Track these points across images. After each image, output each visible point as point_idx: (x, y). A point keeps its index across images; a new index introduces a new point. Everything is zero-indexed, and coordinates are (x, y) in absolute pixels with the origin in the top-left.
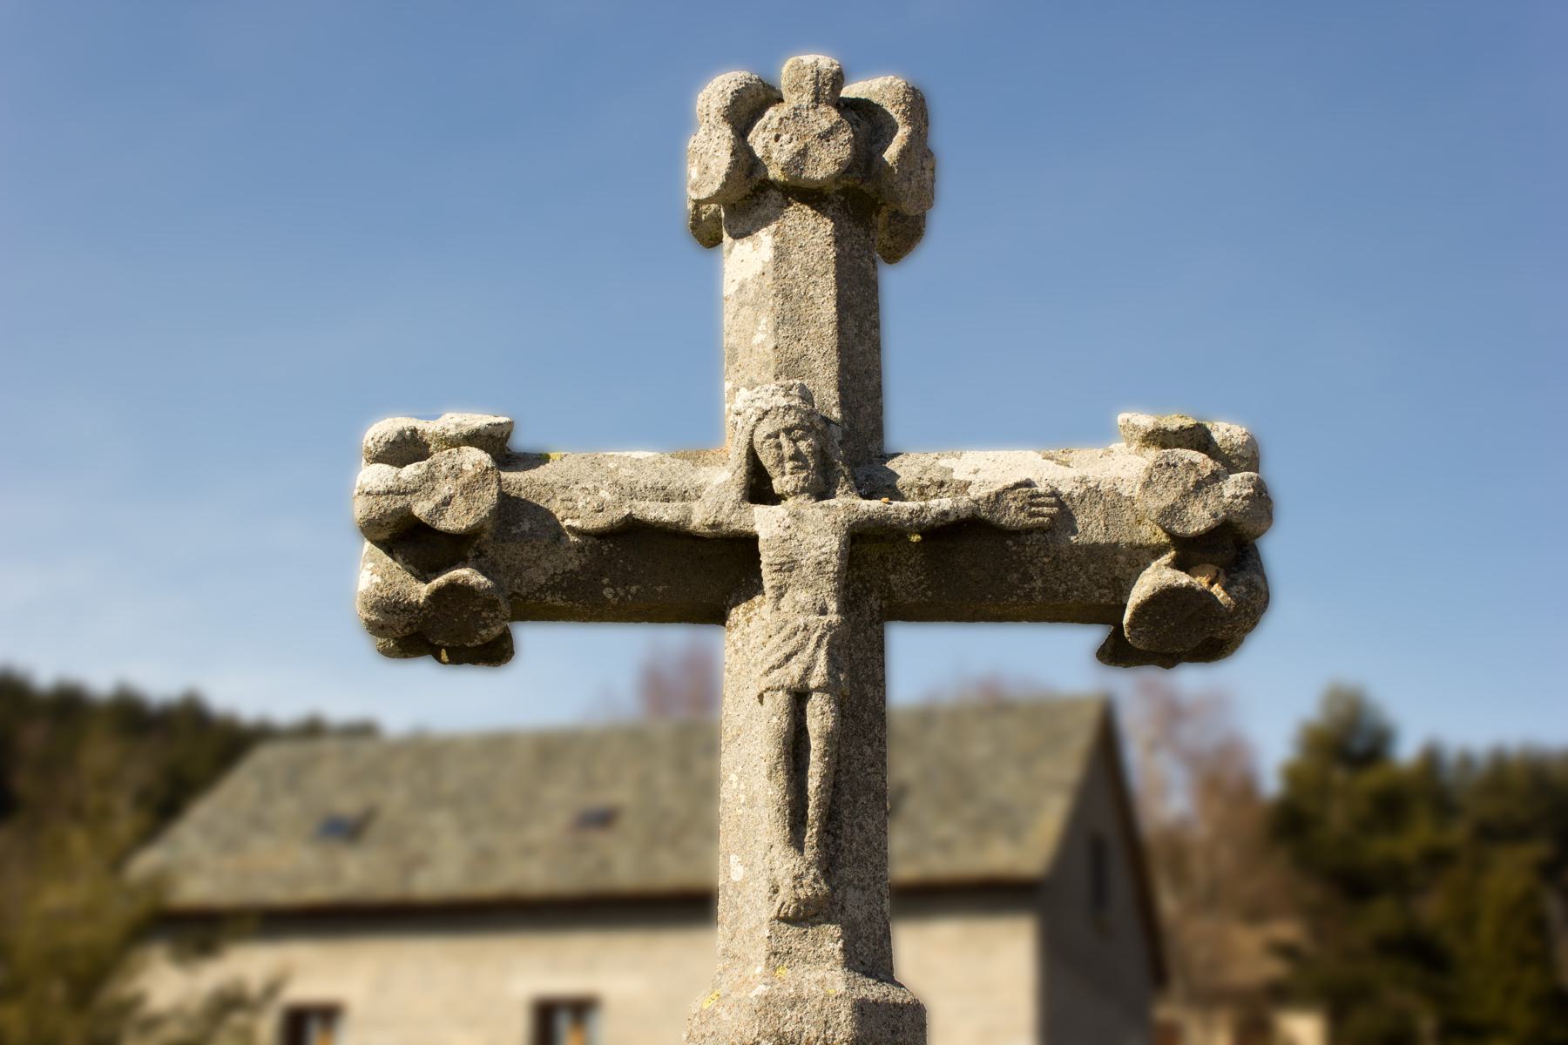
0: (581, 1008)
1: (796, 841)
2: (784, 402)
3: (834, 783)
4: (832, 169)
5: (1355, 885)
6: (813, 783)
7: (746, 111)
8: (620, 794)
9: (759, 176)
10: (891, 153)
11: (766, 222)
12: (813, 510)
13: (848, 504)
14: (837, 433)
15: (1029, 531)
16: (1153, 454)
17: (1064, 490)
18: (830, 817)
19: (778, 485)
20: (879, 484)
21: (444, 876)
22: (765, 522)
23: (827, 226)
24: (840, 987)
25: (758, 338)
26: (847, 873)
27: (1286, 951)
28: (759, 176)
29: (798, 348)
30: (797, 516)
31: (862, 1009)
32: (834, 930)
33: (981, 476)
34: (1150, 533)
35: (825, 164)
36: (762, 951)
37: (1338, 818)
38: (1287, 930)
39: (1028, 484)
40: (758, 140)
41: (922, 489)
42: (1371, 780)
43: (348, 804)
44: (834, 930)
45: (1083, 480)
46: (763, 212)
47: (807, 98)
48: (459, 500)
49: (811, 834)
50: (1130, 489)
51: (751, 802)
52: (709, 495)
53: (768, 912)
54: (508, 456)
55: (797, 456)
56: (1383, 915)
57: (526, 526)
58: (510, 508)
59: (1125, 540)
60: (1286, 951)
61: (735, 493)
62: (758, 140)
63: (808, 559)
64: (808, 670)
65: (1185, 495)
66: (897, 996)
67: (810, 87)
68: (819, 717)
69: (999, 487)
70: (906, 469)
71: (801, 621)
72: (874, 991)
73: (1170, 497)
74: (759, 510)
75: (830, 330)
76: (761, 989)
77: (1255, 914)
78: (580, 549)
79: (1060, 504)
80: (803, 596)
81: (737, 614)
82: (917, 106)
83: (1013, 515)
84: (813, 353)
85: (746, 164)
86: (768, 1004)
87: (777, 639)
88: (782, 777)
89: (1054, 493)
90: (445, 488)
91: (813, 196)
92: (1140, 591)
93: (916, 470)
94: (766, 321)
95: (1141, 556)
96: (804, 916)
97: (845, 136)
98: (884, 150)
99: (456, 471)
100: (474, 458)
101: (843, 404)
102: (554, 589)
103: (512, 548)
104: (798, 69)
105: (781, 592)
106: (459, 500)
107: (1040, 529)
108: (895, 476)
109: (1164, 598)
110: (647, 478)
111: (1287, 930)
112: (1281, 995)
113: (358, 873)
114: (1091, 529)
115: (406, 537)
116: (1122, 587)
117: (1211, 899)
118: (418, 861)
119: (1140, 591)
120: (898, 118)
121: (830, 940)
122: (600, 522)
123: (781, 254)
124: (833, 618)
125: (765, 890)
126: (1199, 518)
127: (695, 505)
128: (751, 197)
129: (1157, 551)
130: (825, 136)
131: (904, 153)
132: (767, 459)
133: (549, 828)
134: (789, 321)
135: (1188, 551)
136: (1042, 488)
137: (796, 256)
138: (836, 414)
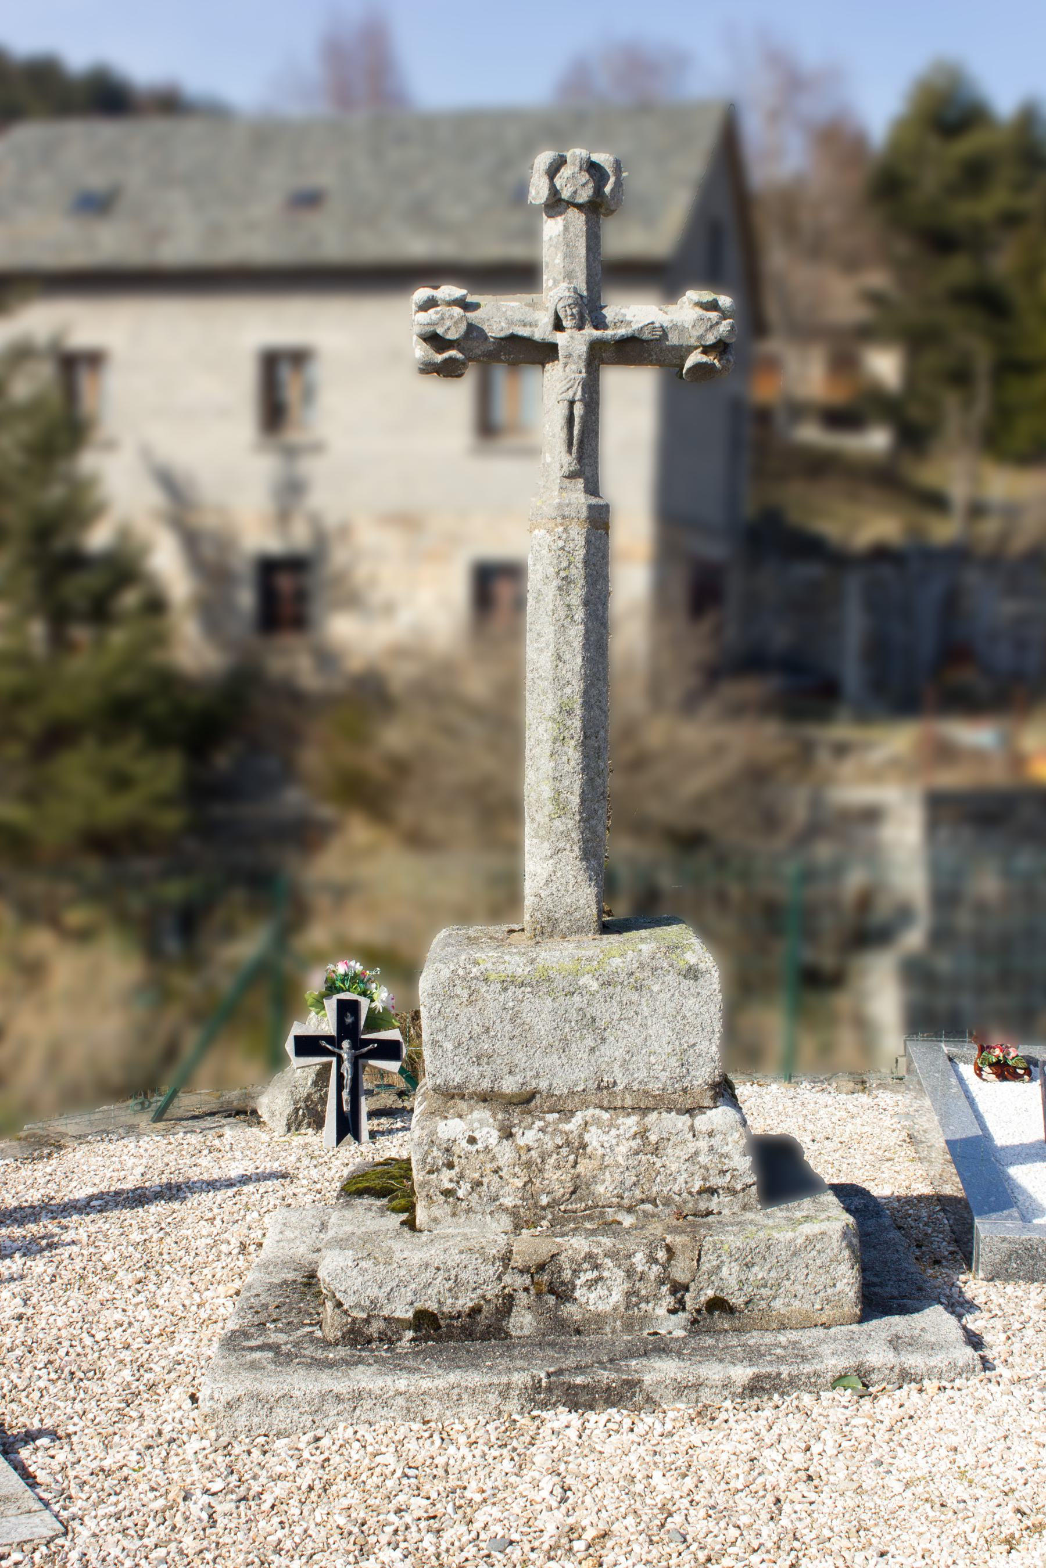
0: (299, 357)
1: (570, 451)
2: (568, 294)
3: (582, 432)
4: (586, 199)
5: (941, 242)
6: (576, 432)
7: (553, 171)
8: (324, 178)
9: (558, 197)
10: (607, 189)
11: (560, 214)
12: (577, 334)
13: (591, 333)
14: (585, 300)
15: (652, 340)
16: (700, 312)
17: (665, 325)
18: (581, 442)
19: (565, 323)
20: (600, 323)
21: (181, 249)
22: (561, 339)
23: (583, 217)
24: (583, 500)
25: (557, 261)
26: (586, 461)
27: (875, 299)
28: (558, 197)
29: (572, 267)
30: (572, 337)
31: (590, 507)
32: (581, 480)
33: (636, 318)
34: (693, 342)
35: (584, 196)
36: (557, 487)
37: (930, 182)
38: (878, 279)
39: (653, 323)
40: (558, 182)
41: (615, 323)
42: (966, 146)
43: (96, 180)
44: (581, 480)
45: (672, 321)
46: (557, 209)
47: (577, 169)
48: (453, 328)
49: (574, 449)
50: (688, 325)
51: (554, 436)
52: (541, 330)
53: (560, 474)
54: (343, 96)
55: (572, 315)
56: (958, 270)
57: (475, 334)
58: (471, 328)
59: (685, 344)
60: (875, 299)
61: (550, 327)
62: (558, 182)
63: (575, 354)
64: (575, 394)
65: (706, 330)
66: (601, 502)
67: (578, 164)
68: (578, 410)
69: (642, 325)
70: (610, 313)
71: (573, 376)
72: (594, 501)
73: (701, 331)
74: (559, 334)
75: (583, 260)
76: (557, 501)
77: (851, 264)
78: (494, 343)
79: (664, 330)
80: (574, 367)
81: (548, 366)
82: (618, 167)
83: (646, 335)
84: (577, 269)
85: (554, 192)
86: (560, 506)
87: (564, 382)
88: (565, 430)
89: (662, 327)
90: (448, 323)
91: (579, 207)
92: (689, 363)
93: (613, 314)
94: (560, 256)
95: (690, 349)
96: (572, 476)
97: (591, 185)
98: (605, 186)
99: (451, 317)
100: (457, 311)
101: (588, 289)
102: (484, 356)
103: (470, 342)
104: (576, 154)
105: (566, 365)
106: (453, 328)
107: (656, 340)
108: (605, 317)
109: (698, 367)
110: (518, 316)
111: (878, 279)
112: (867, 334)
113: (110, 243)
114: (673, 339)
115: (434, 340)
116: (683, 359)
117: (816, 250)
118: (158, 235)
119: (689, 363)
120: (610, 173)
121: (580, 483)
122: (502, 335)
123: (566, 229)
124: (584, 375)
125: (559, 467)
126: (711, 339)
127: (536, 330)
128: (556, 204)
129: (696, 348)
130: (583, 185)
131: (612, 190)
132: (562, 315)
133: (266, 207)
134: (569, 256)
135: (706, 350)
136: (657, 325)
137: (571, 229)
138: (585, 294)
